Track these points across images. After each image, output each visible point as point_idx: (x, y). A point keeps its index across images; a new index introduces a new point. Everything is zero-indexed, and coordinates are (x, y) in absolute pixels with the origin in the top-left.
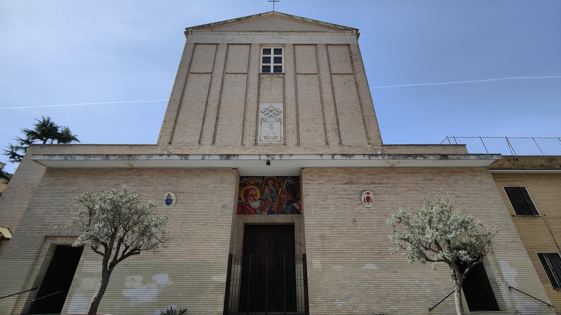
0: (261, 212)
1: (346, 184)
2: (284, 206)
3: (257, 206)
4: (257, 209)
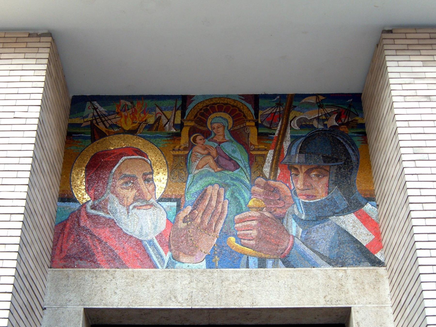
0: (175, 258)
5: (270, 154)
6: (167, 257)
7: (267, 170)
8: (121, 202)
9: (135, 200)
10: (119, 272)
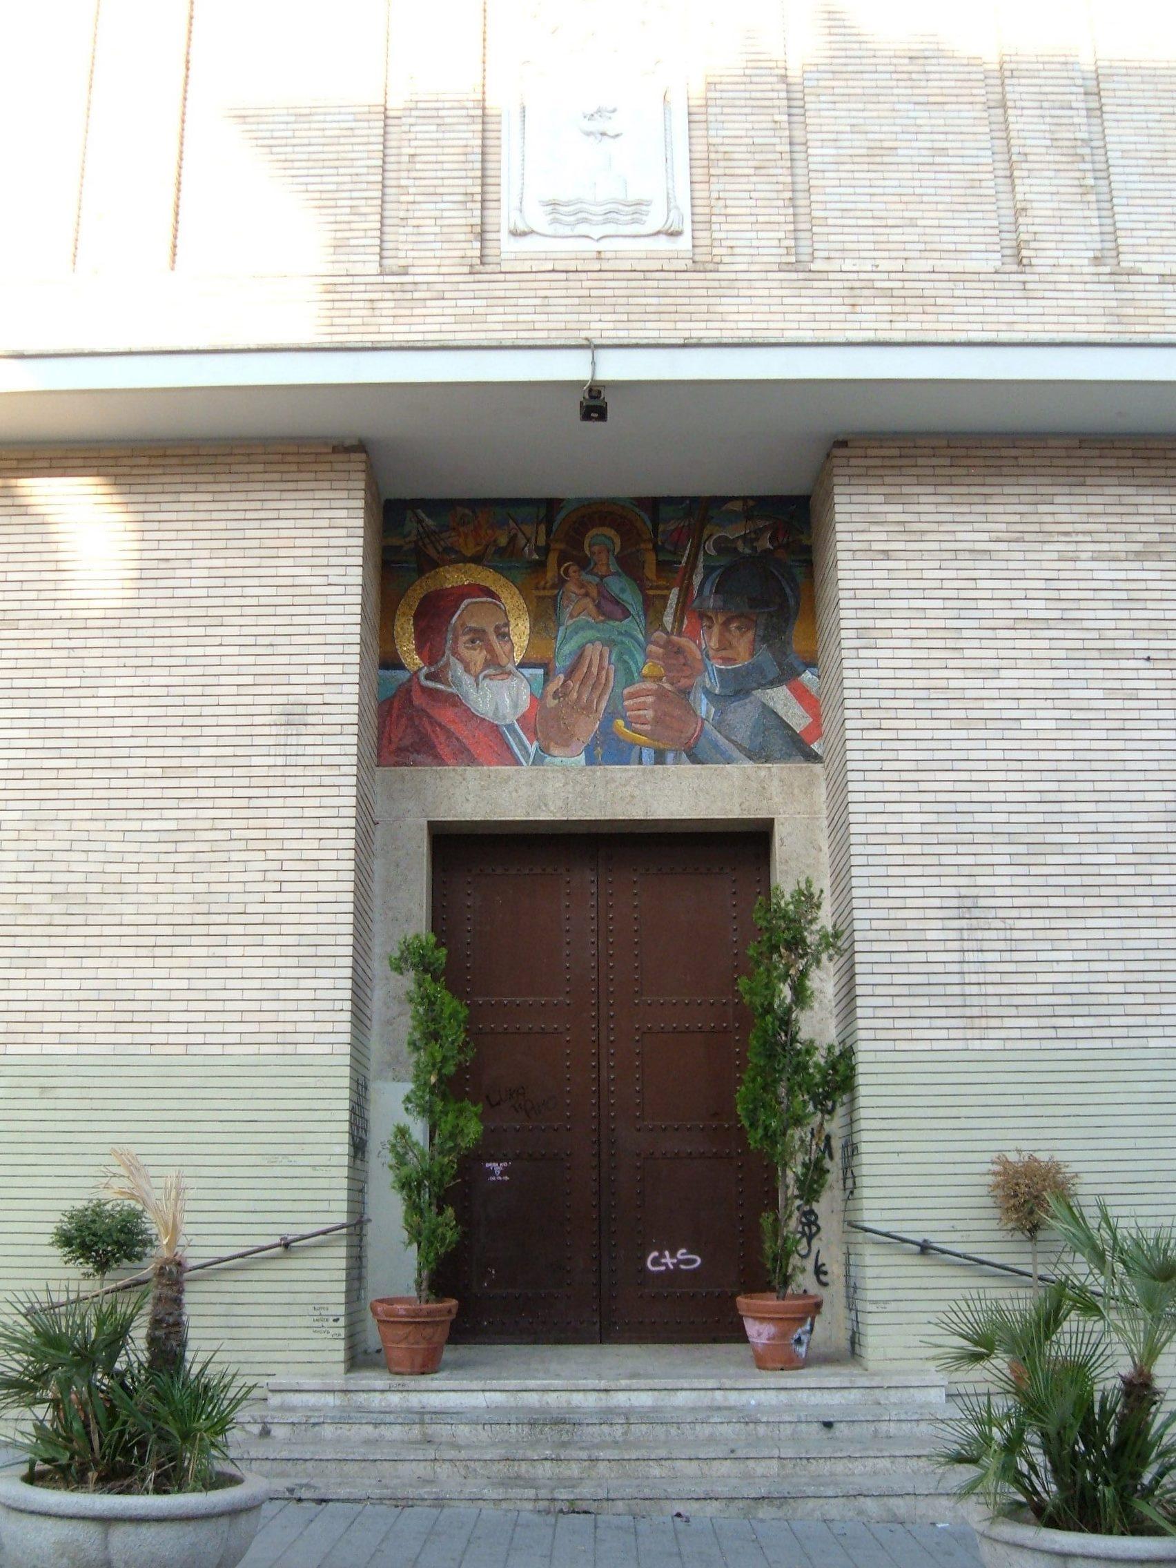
0: (544, 750)
1: (1139, 556)
2: (704, 707)
3: (515, 705)
4: (510, 727)
5: (674, 595)
6: (533, 748)
7: (668, 620)
8: (467, 669)
9: (487, 664)
10: (471, 771)
